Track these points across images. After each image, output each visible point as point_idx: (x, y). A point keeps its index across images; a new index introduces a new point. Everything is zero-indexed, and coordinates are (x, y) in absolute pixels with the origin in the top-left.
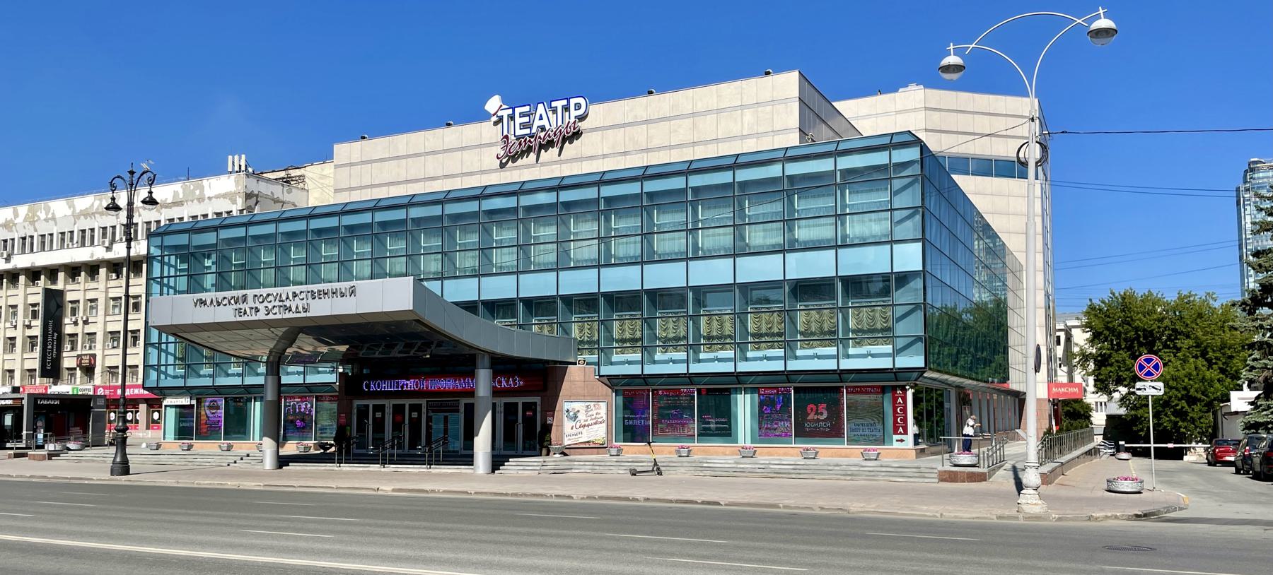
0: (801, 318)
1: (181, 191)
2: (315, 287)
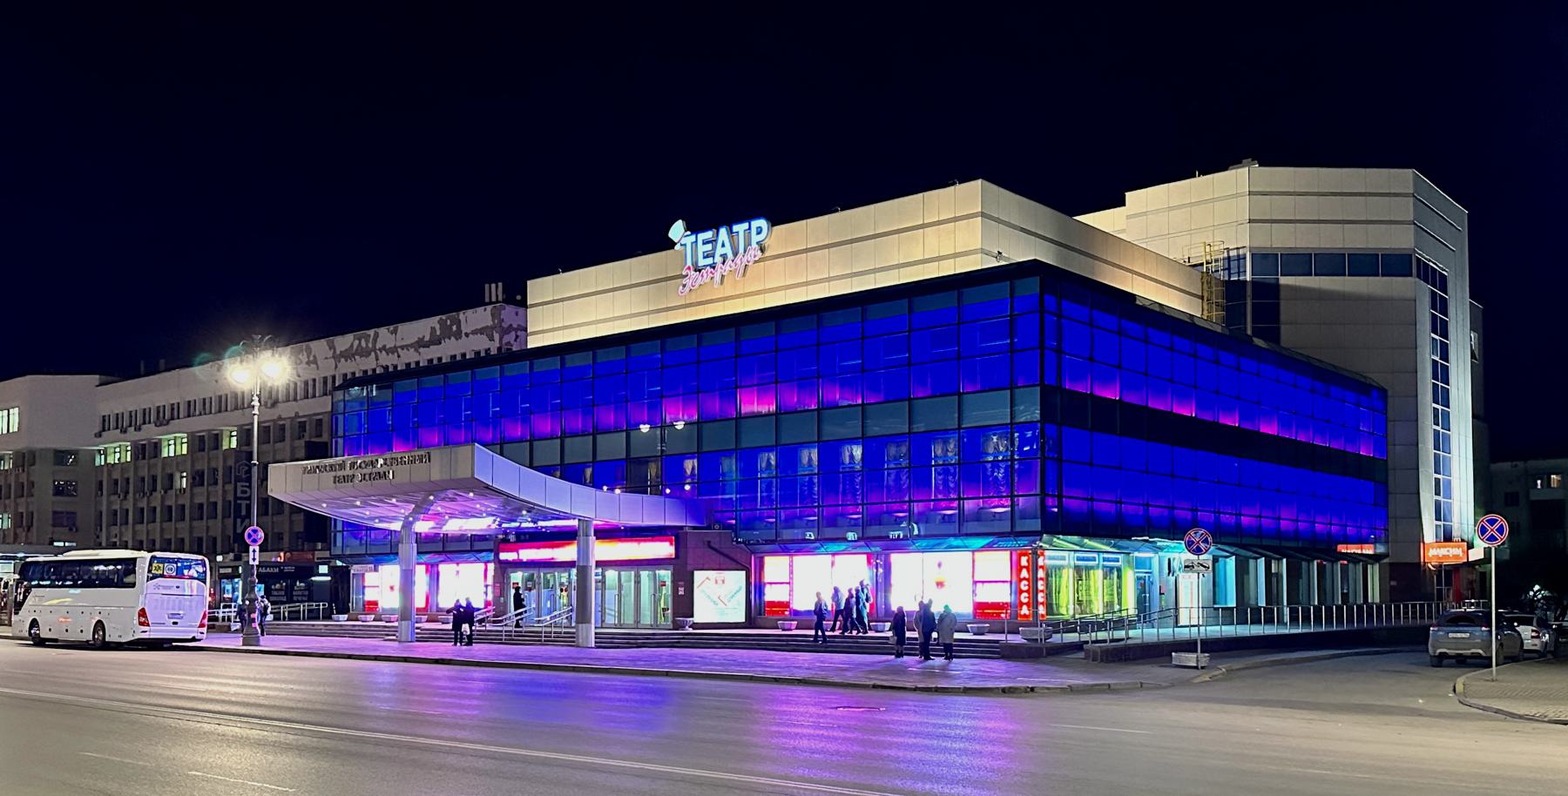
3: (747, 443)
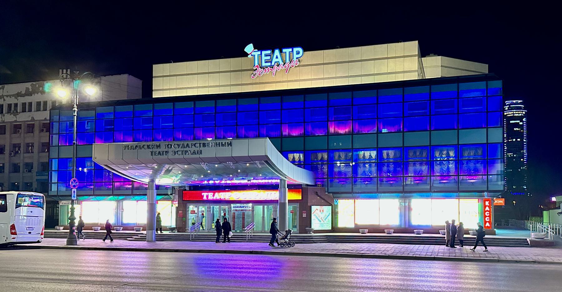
1: (30, 87)
3: (331, 147)
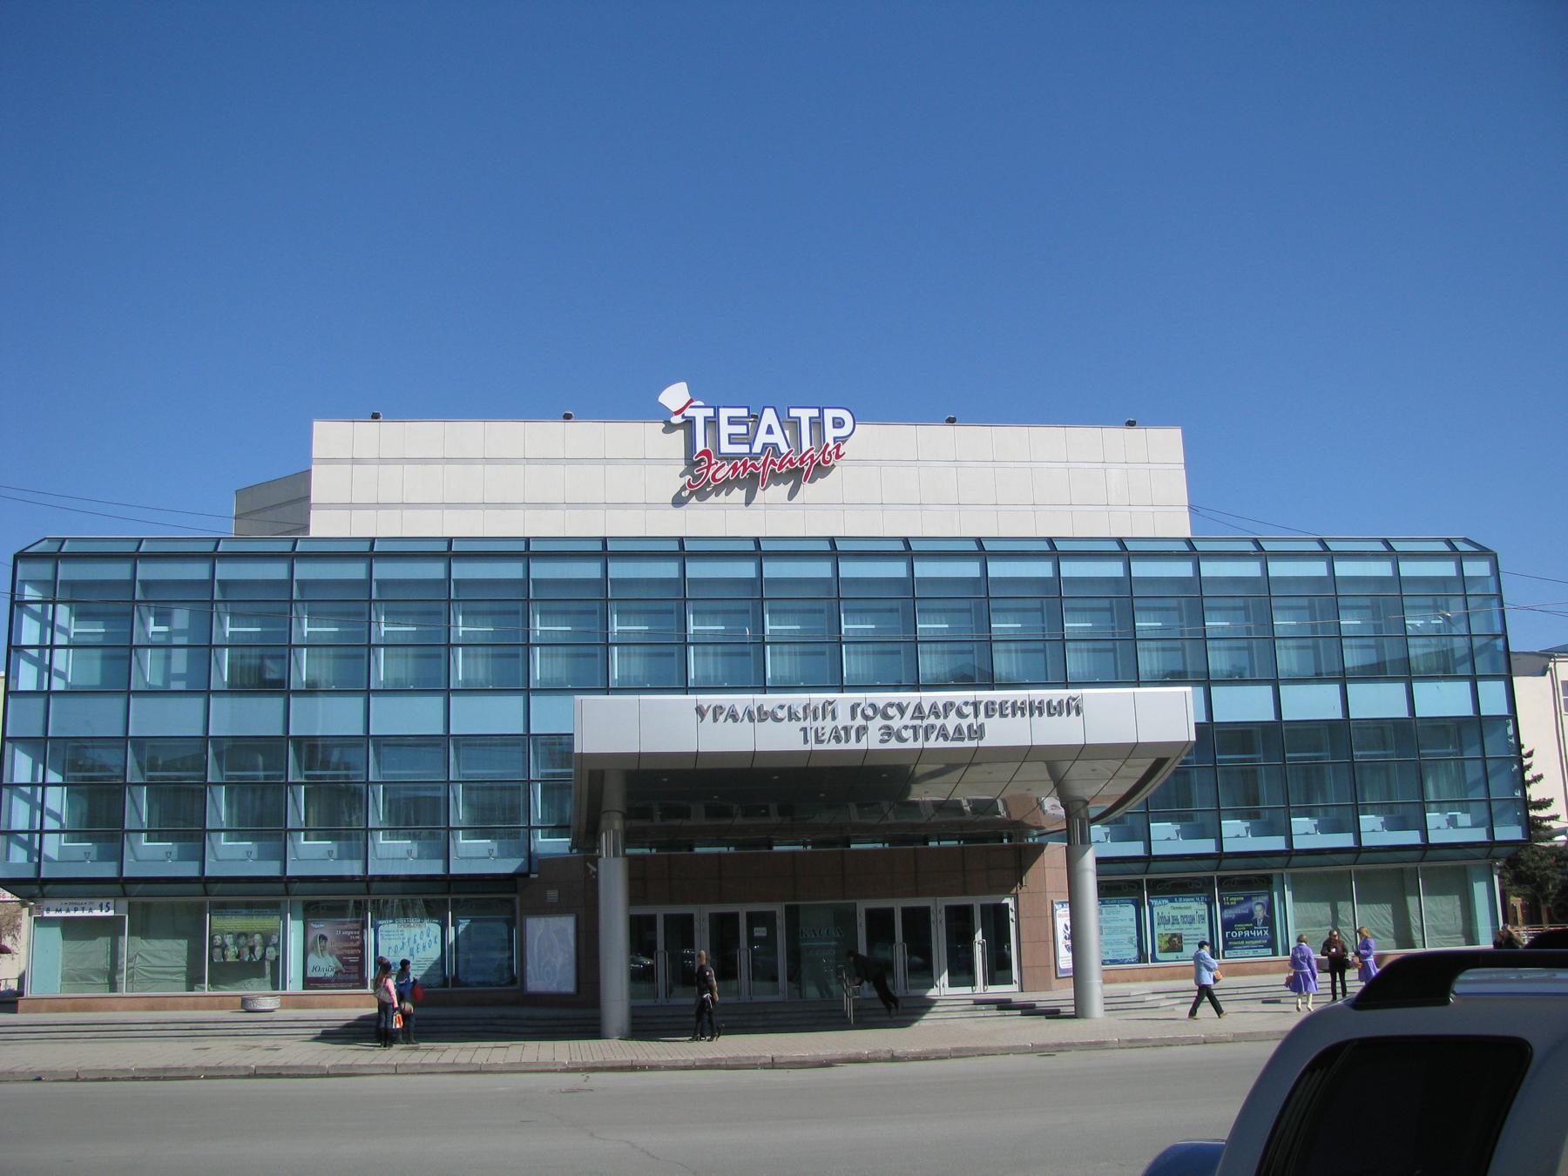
0: (406, 935)
2: (985, 695)
